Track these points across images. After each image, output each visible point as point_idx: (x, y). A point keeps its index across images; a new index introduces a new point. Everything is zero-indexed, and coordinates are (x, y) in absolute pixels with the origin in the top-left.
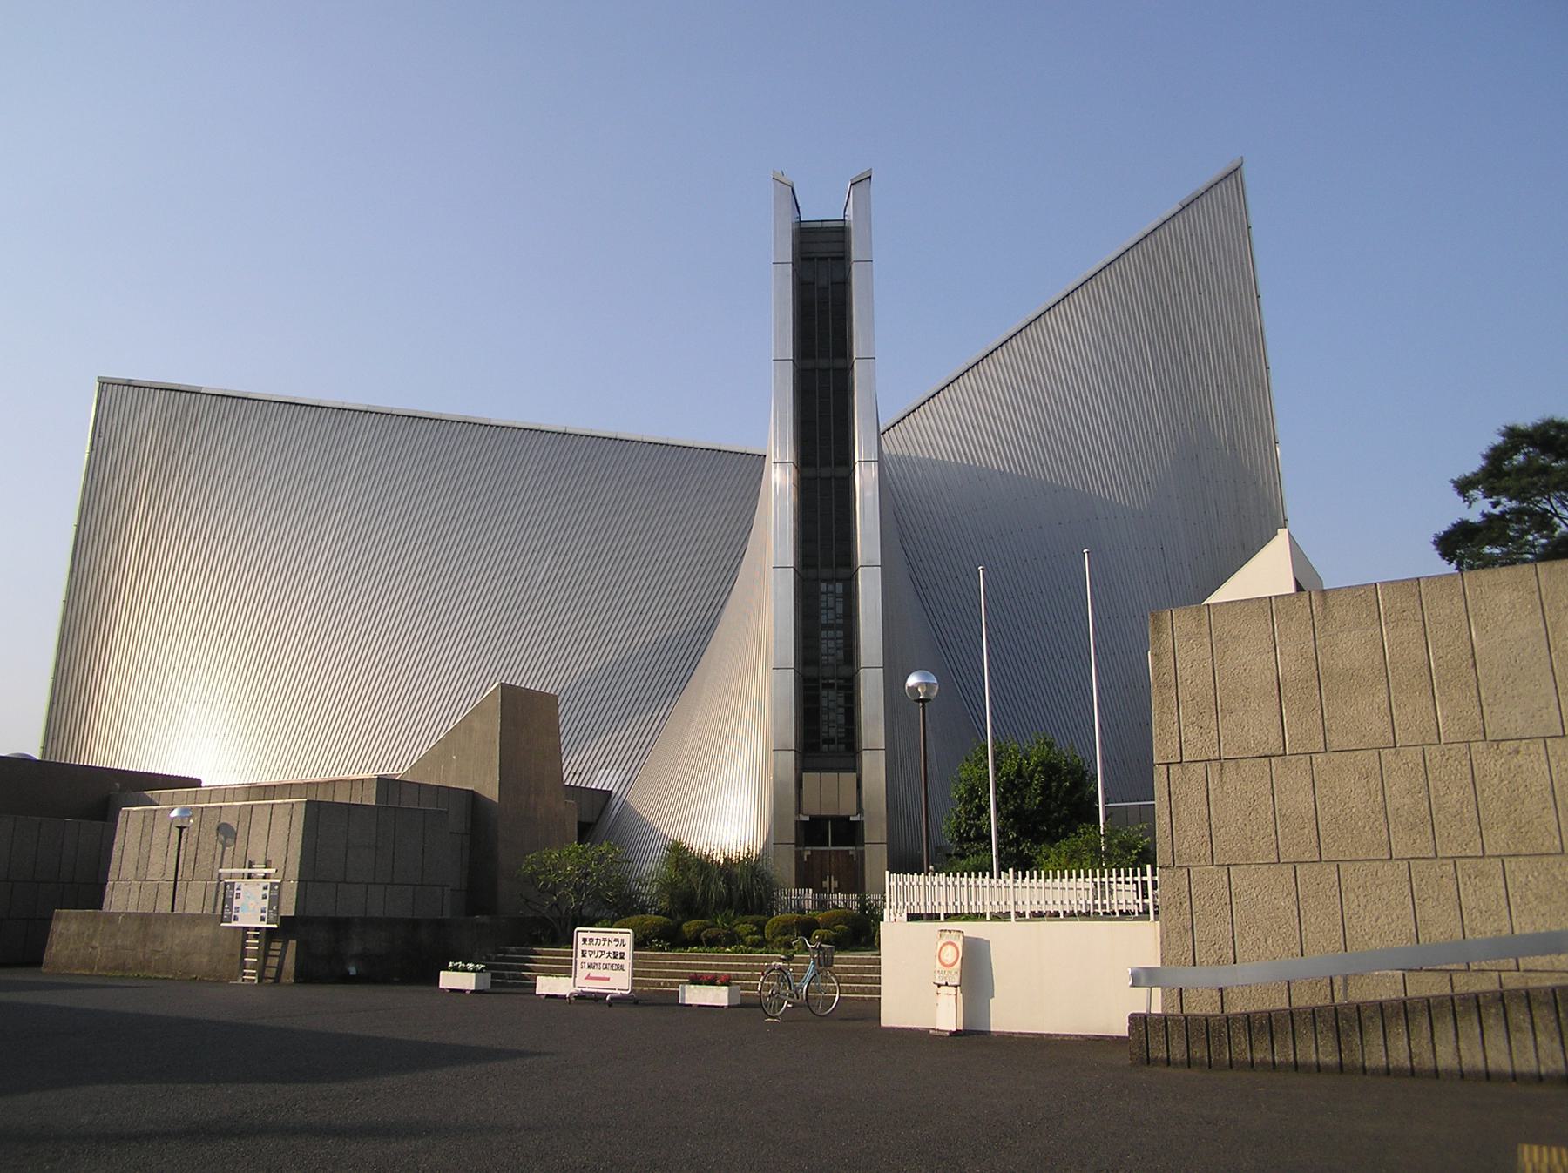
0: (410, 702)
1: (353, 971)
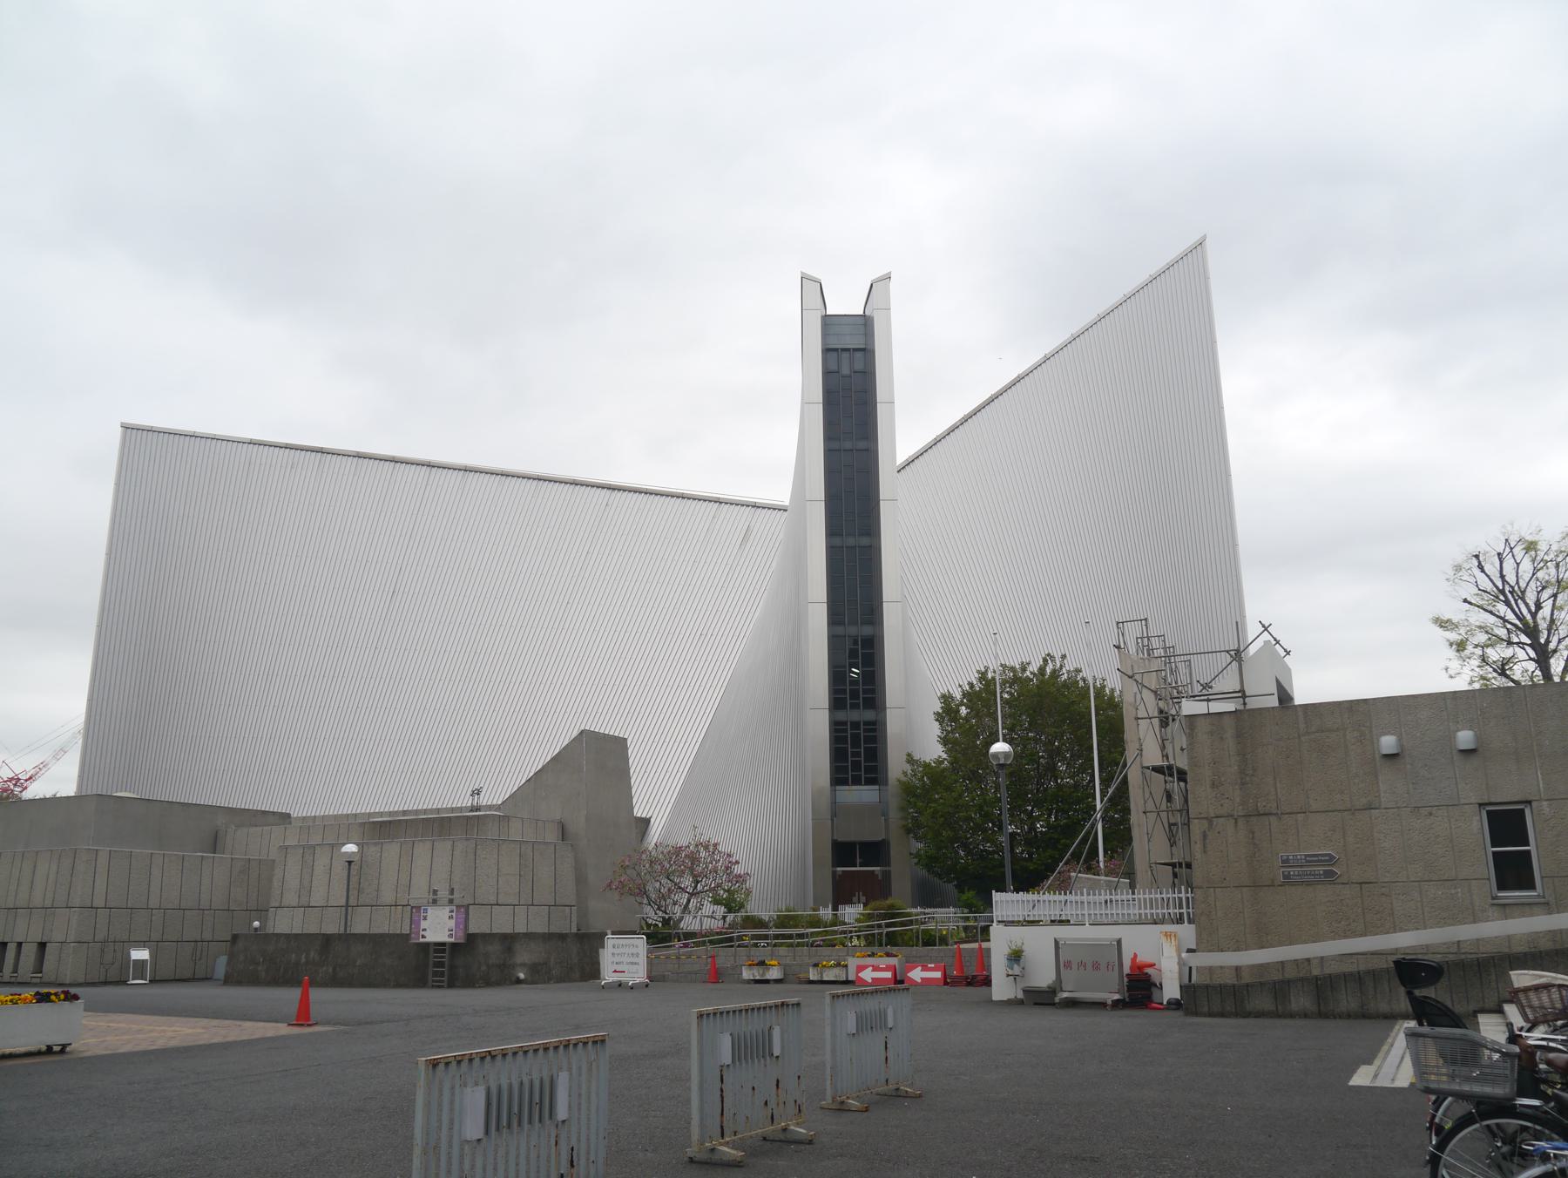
0: (658, 774)
1: (522, 976)
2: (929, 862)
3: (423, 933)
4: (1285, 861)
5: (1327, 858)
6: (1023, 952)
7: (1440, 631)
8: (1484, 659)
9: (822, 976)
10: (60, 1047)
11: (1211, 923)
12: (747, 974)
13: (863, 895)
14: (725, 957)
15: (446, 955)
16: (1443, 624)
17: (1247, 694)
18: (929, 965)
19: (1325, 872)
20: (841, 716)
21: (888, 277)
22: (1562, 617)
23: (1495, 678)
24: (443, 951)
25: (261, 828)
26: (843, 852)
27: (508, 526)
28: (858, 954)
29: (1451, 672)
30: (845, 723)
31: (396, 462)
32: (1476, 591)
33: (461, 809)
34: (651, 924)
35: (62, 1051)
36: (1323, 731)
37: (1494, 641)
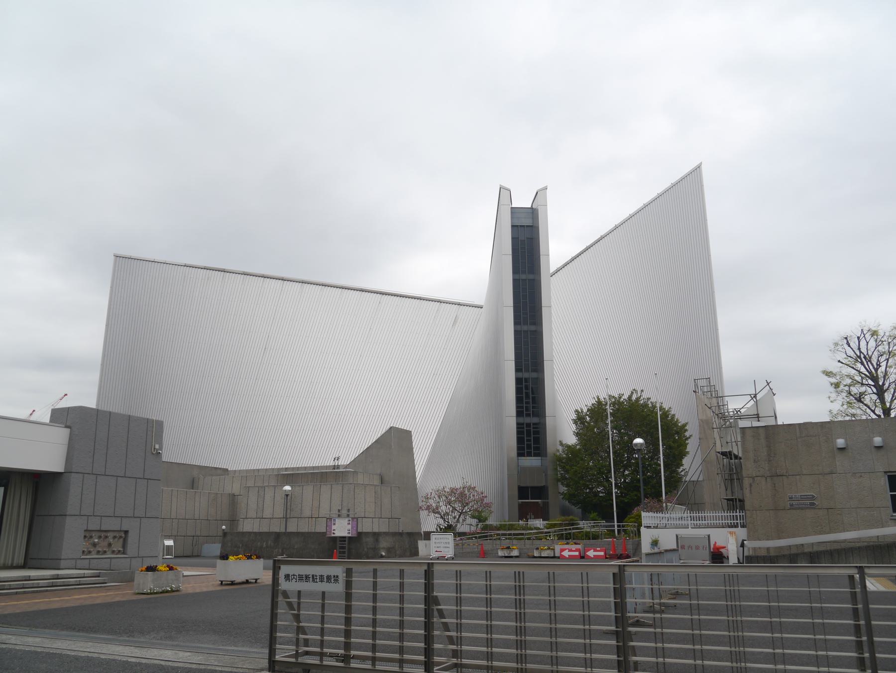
1: (384, 554)
2: (571, 497)
3: (334, 532)
4: (791, 498)
5: (811, 497)
6: (658, 541)
7: (826, 378)
8: (850, 393)
9: (541, 554)
12: (500, 553)
14: (488, 545)
16: (828, 374)
17: (760, 416)
18: (598, 549)
19: (811, 504)
20: (521, 420)
21: (546, 188)
22: (892, 371)
23: (855, 403)
24: (345, 541)
25: (219, 477)
26: (523, 492)
27: (327, 313)
28: (560, 543)
29: (832, 399)
32: (846, 356)
33: (327, 467)
34: (442, 529)
35: (256, 582)
36: (808, 436)
37: (854, 383)
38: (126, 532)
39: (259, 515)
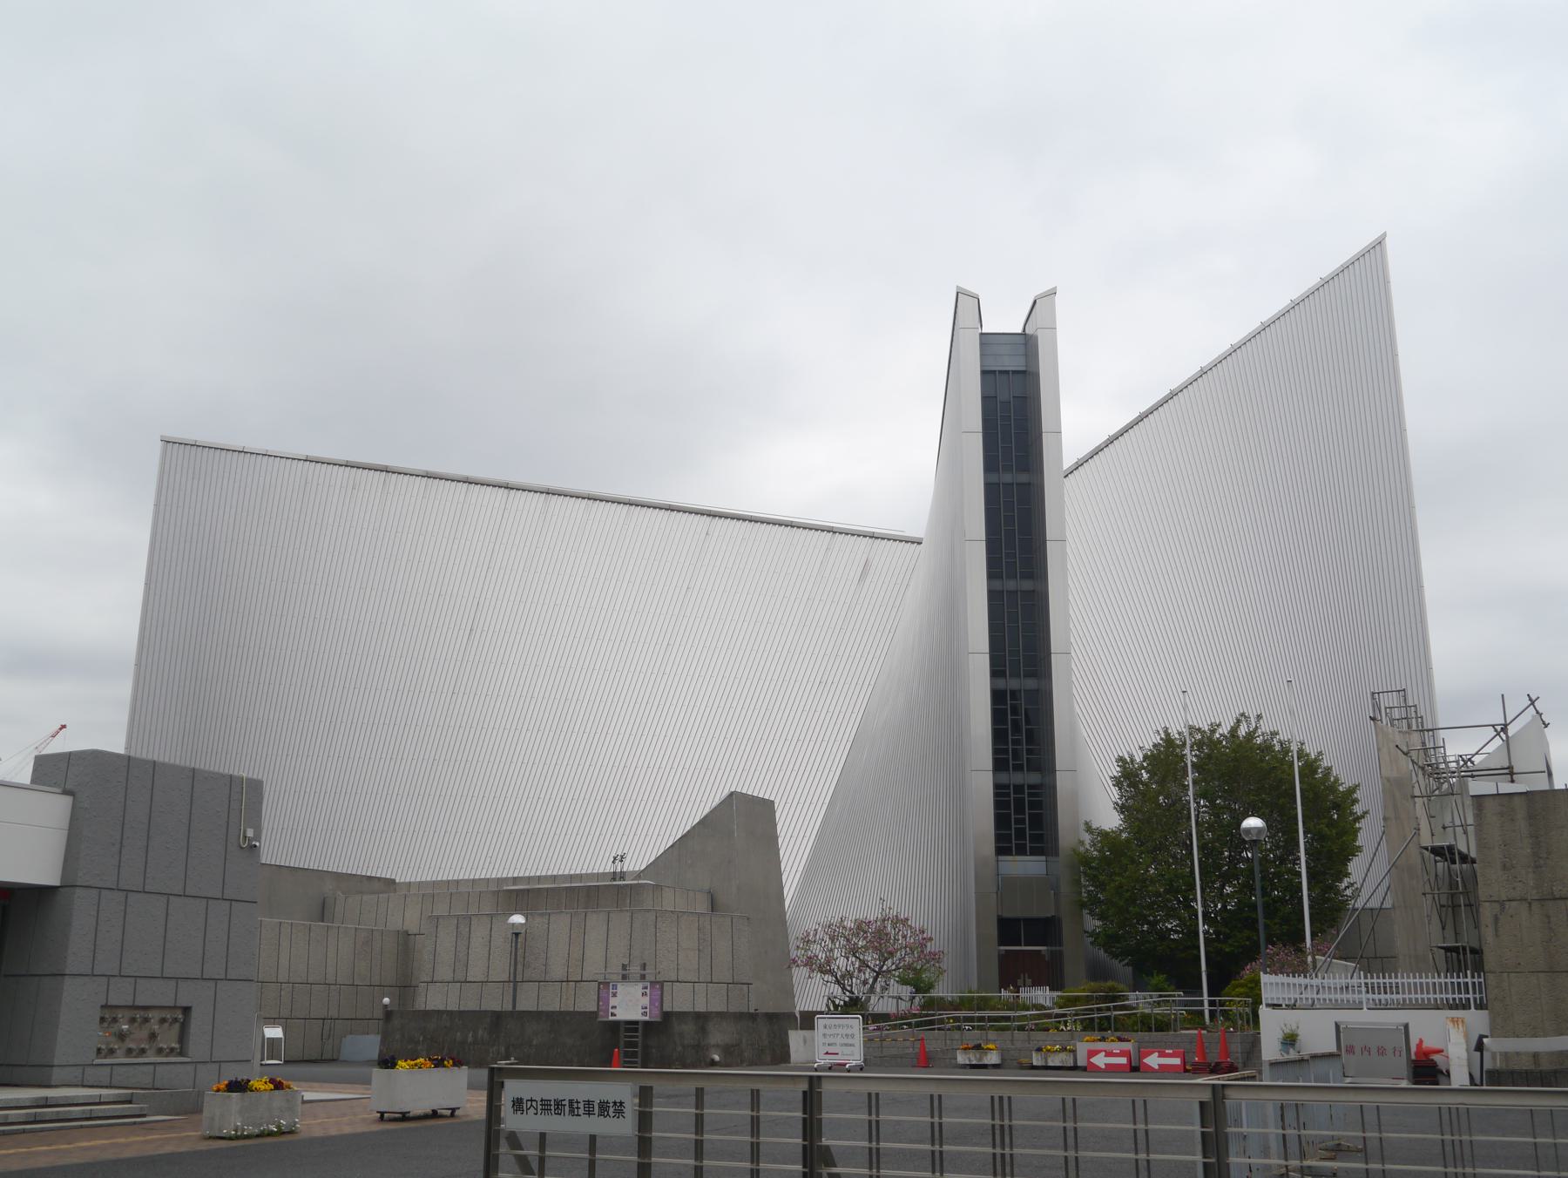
1: (717, 1058)
3: (613, 1011)
9: (1046, 1061)
10: (450, 1111)
11: (1506, 1009)
12: (961, 1058)
13: (1029, 978)
15: (639, 1034)
17: (1515, 771)
18: (1167, 1051)
20: (1004, 778)
21: (1053, 293)
26: (1008, 929)
28: (1087, 1038)
30: (1008, 787)
31: (470, 483)
33: (598, 876)
34: (838, 1005)
35: (452, 1115)
38: (186, 1010)
39: (460, 976)
